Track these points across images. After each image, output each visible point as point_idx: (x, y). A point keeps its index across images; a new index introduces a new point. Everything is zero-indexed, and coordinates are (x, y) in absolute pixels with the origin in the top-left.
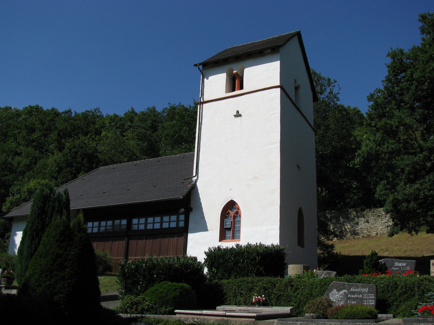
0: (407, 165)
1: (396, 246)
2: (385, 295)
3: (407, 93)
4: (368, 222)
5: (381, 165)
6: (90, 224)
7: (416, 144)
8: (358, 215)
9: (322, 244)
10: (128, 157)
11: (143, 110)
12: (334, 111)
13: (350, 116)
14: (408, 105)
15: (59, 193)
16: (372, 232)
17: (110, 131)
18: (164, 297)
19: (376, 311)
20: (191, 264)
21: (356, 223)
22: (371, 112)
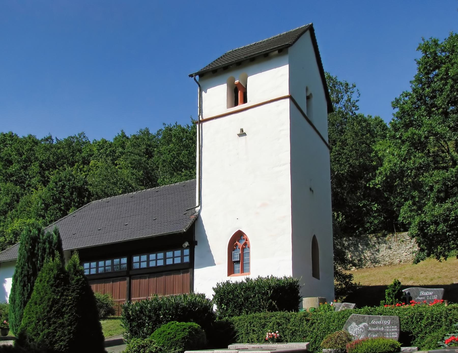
0: (437, 182)
1: (422, 273)
2: (409, 327)
3: (440, 95)
4: (390, 248)
5: (406, 183)
6: (86, 265)
7: (448, 156)
8: (379, 241)
9: (339, 274)
10: (123, 188)
11: (135, 133)
12: (352, 123)
13: (370, 128)
14: (441, 110)
15: (49, 233)
16: (395, 259)
17: (99, 160)
18: (173, 338)
19: (399, 344)
20: (199, 301)
21: (376, 250)
22: (396, 121)
